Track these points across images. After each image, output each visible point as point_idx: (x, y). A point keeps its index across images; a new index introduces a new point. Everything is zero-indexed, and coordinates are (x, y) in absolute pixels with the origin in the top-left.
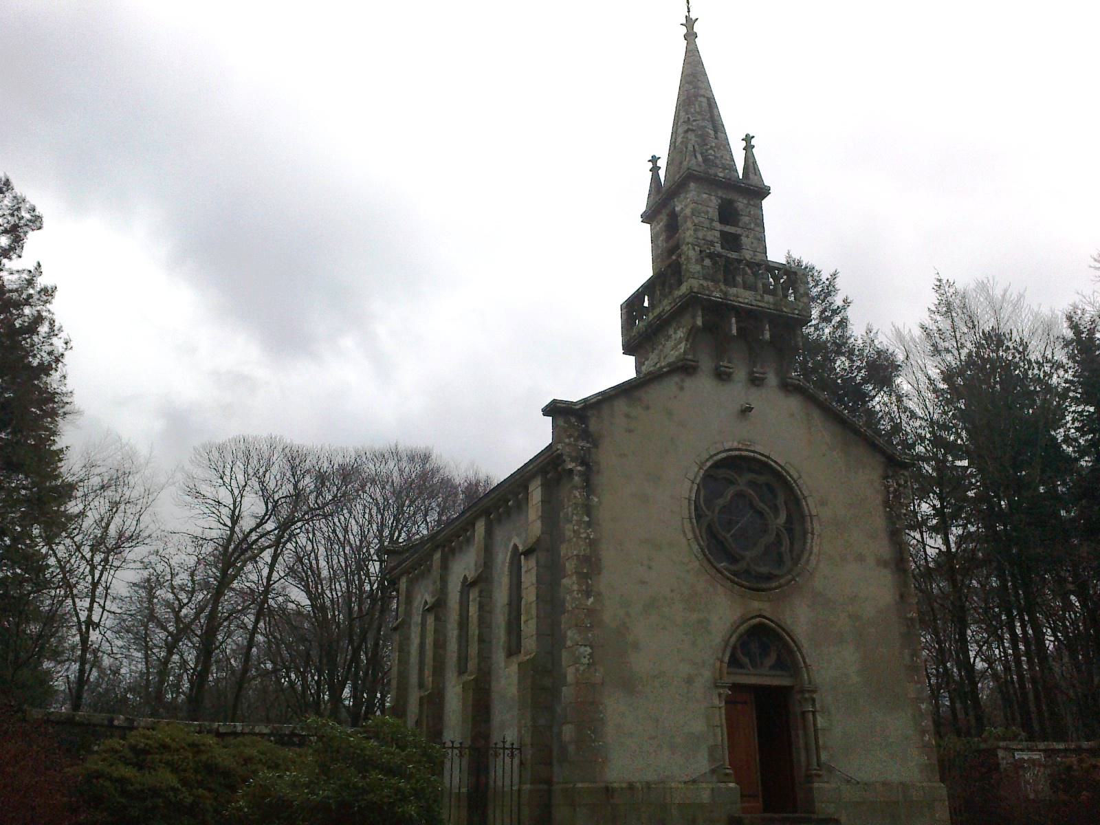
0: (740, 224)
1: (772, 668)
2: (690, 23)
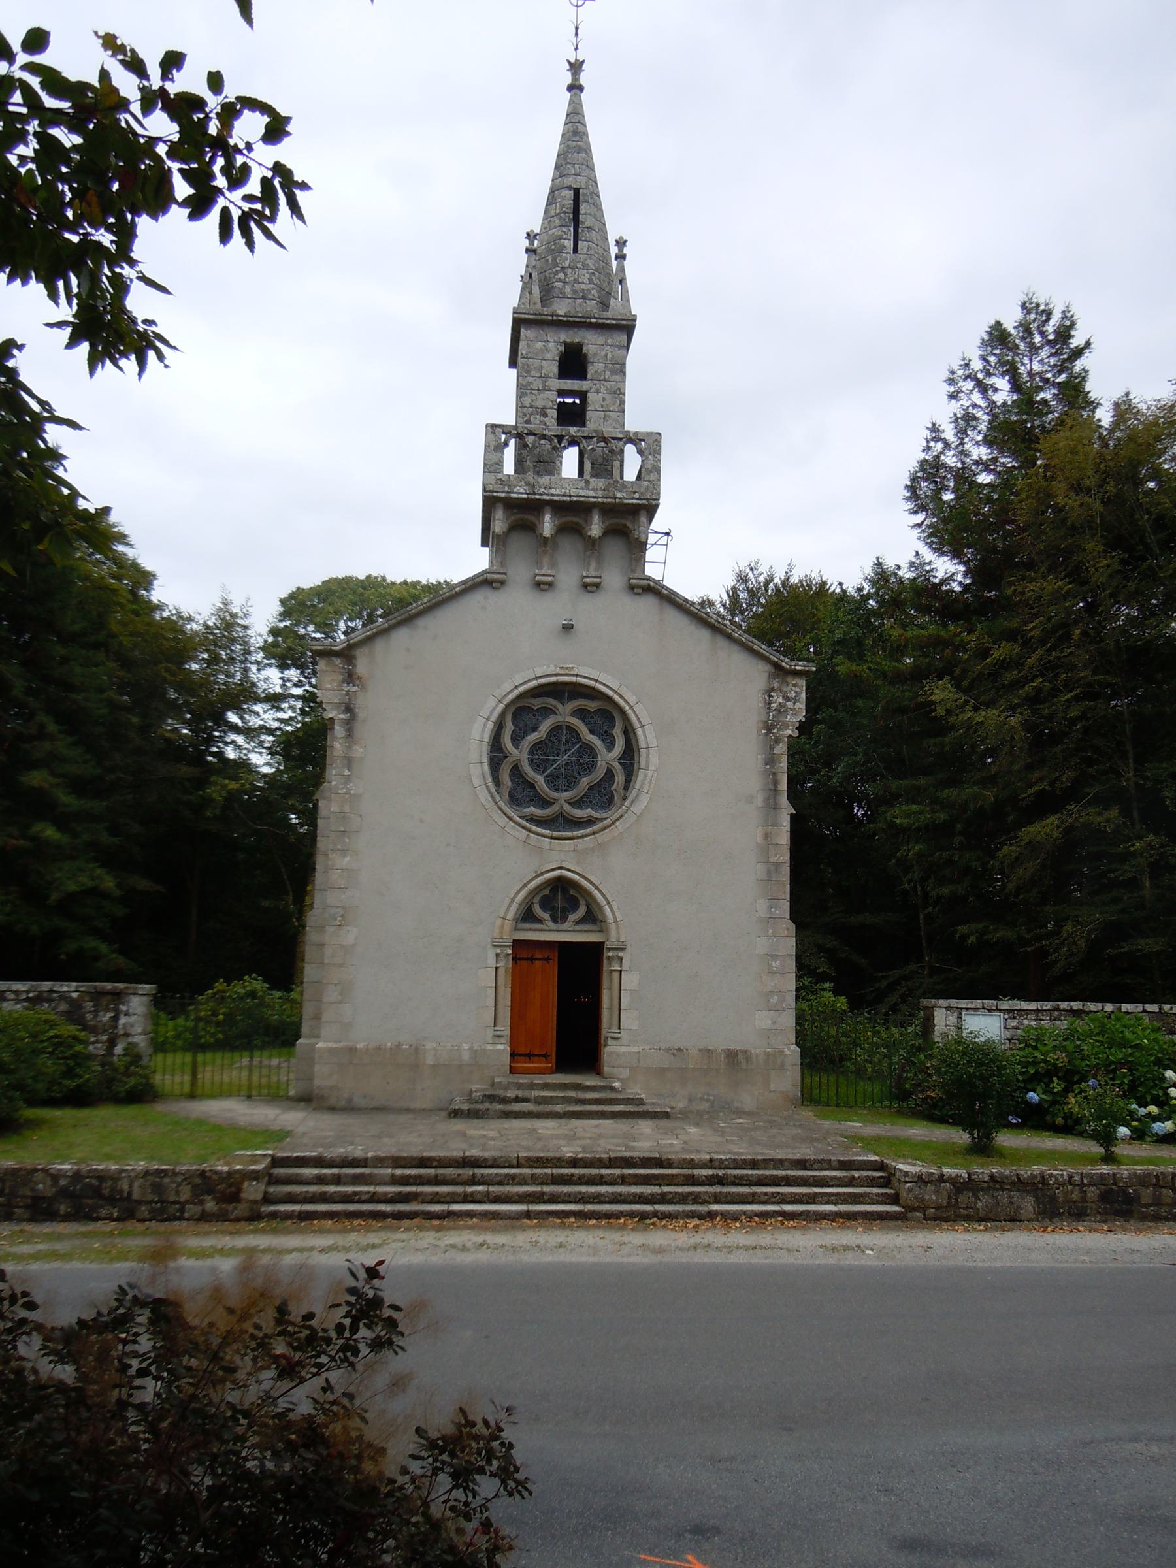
0: (589, 376)
1: (578, 922)
2: (163, 289)
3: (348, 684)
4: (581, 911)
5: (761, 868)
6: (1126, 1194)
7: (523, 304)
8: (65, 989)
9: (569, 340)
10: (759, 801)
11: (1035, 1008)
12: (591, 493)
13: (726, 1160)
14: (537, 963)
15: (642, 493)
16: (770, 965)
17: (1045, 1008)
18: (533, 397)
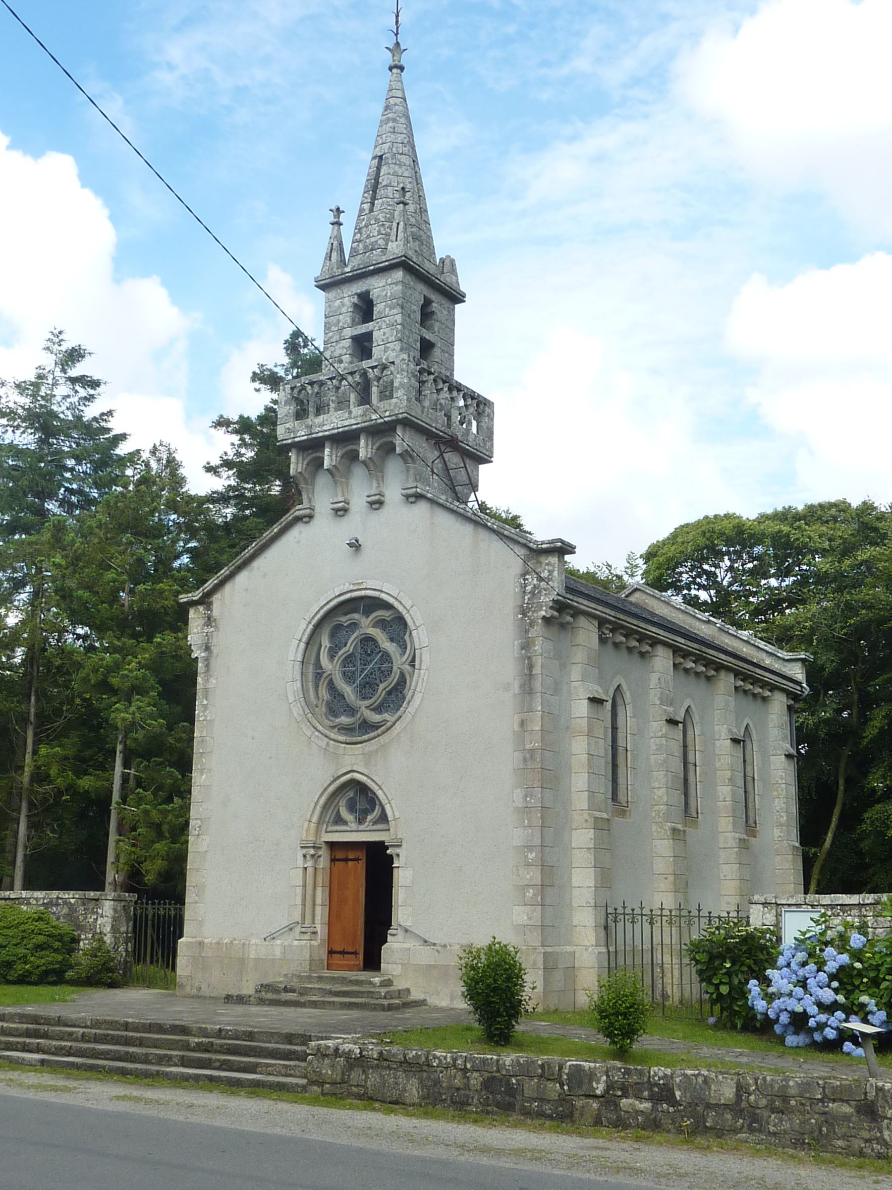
3: (208, 626)
4: (377, 812)
5: (518, 755)
6: (508, 1083)
7: (324, 272)
8: (67, 896)
9: (359, 291)
10: (516, 688)
11: (856, 902)
12: (353, 421)
13: (230, 1030)
14: (350, 863)
15: (392, 410)
16: (526, 857)
17: (867, 902)
18: (333, 349)
